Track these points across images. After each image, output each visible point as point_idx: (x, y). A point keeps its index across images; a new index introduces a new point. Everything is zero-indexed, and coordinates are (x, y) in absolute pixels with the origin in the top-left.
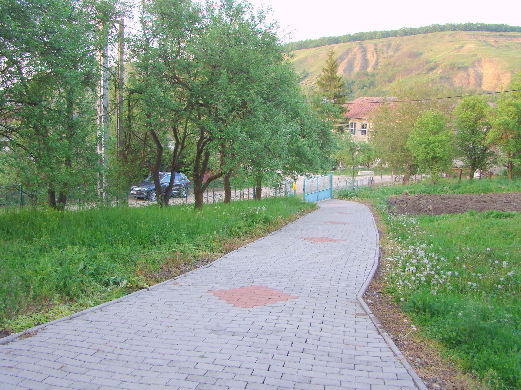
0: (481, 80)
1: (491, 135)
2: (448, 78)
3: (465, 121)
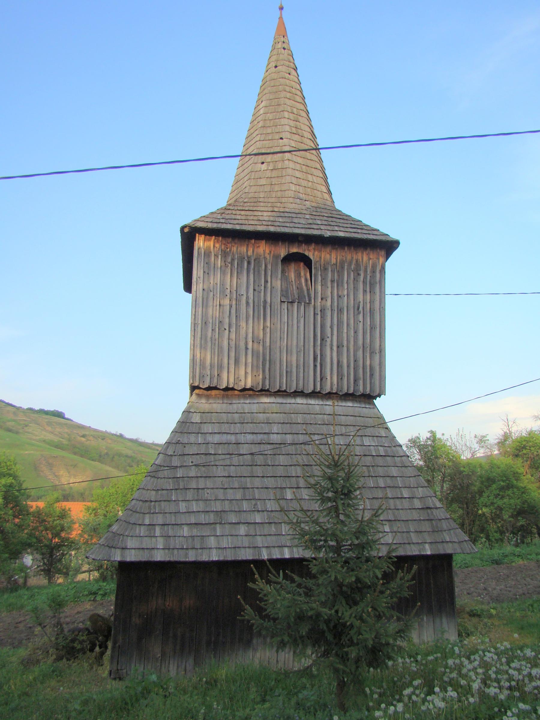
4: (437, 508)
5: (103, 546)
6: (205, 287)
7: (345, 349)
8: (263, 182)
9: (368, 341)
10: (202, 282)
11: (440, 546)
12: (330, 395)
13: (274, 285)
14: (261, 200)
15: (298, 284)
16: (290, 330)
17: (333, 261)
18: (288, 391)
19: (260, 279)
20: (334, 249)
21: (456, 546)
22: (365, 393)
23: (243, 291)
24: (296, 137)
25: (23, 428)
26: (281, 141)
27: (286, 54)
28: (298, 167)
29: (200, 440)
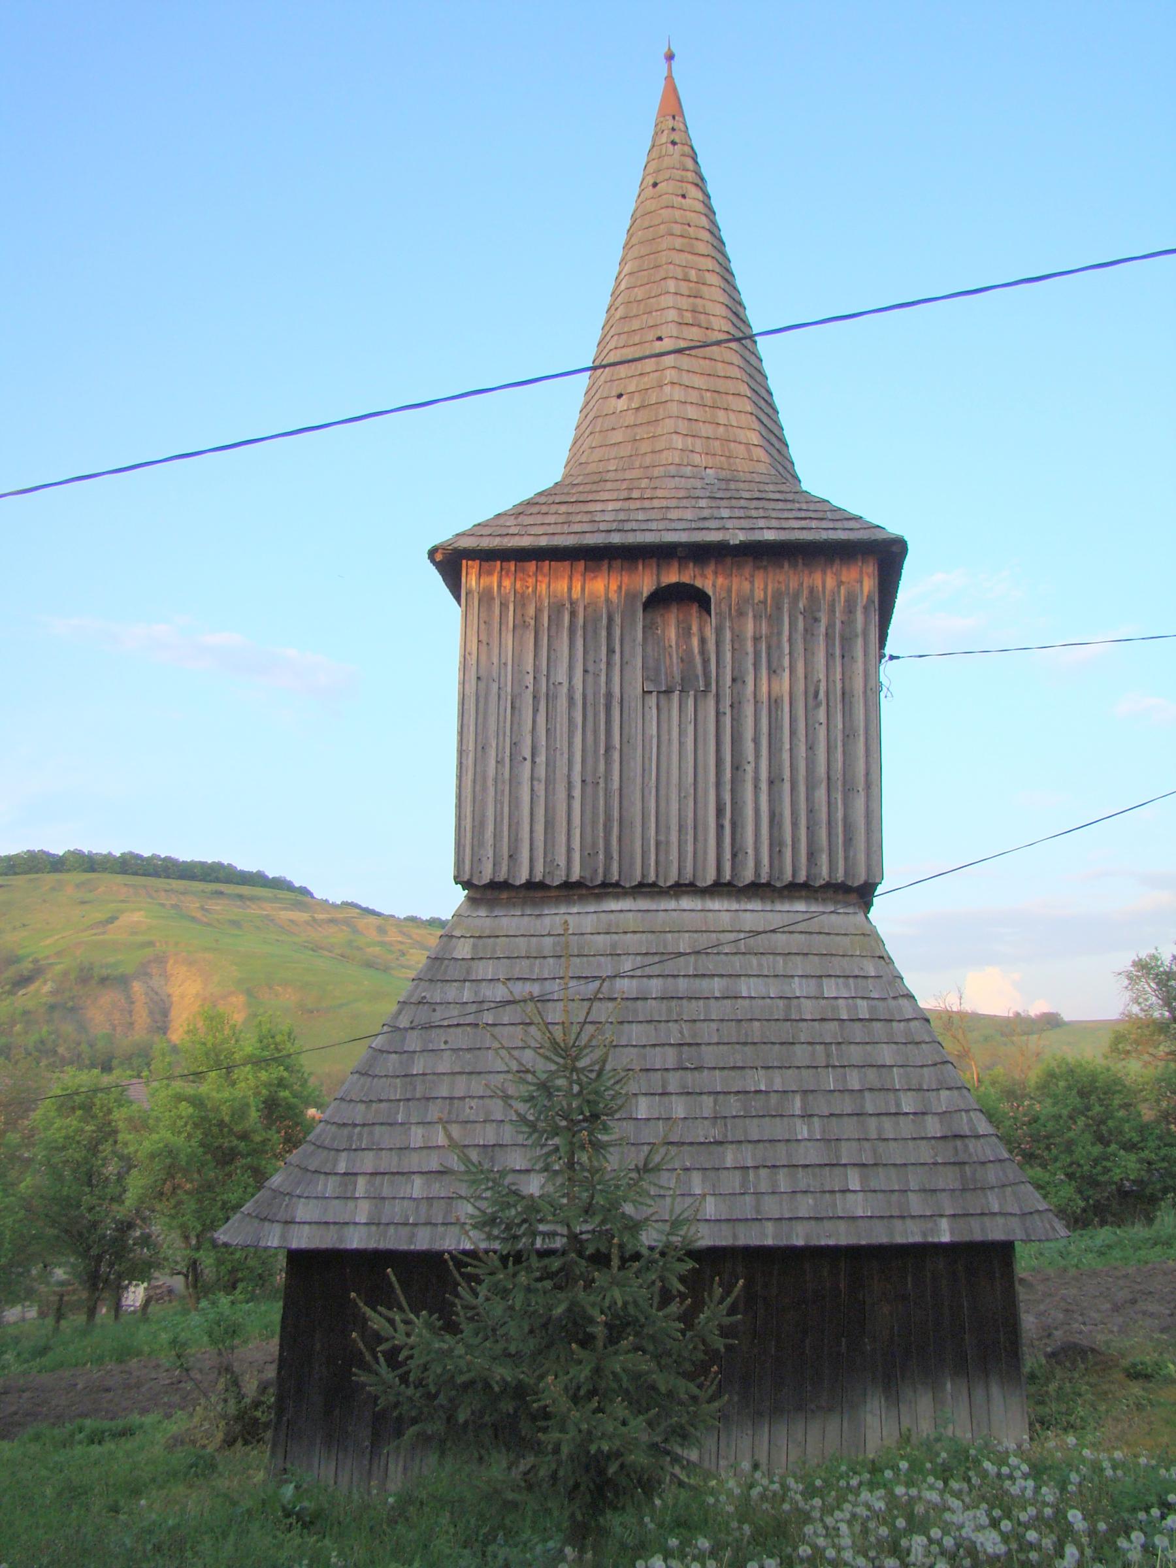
0: (165, 1013)
1: (136, 1185)
2: (72, 1009)
3: (64, 1148)
4: (978, 1137)
5: (248, 1219)
6: (483, 673)
7: (787, 786)
8: (617, 436)
9: (840, 765)
11: (975, 1224)
12: (756, 889)
15: (685, 650)
16: (664, 749)
17: (759, 595)
18: (661, 883)
19: (597, 649)
20: (758, 568)
21: (1015, 1223)
22: (834, 882)
23: (561, 676)
25: (397, 959)
26: (658, 343)
27: (676, 156)
28: (694, 396)
29: (467, 996)
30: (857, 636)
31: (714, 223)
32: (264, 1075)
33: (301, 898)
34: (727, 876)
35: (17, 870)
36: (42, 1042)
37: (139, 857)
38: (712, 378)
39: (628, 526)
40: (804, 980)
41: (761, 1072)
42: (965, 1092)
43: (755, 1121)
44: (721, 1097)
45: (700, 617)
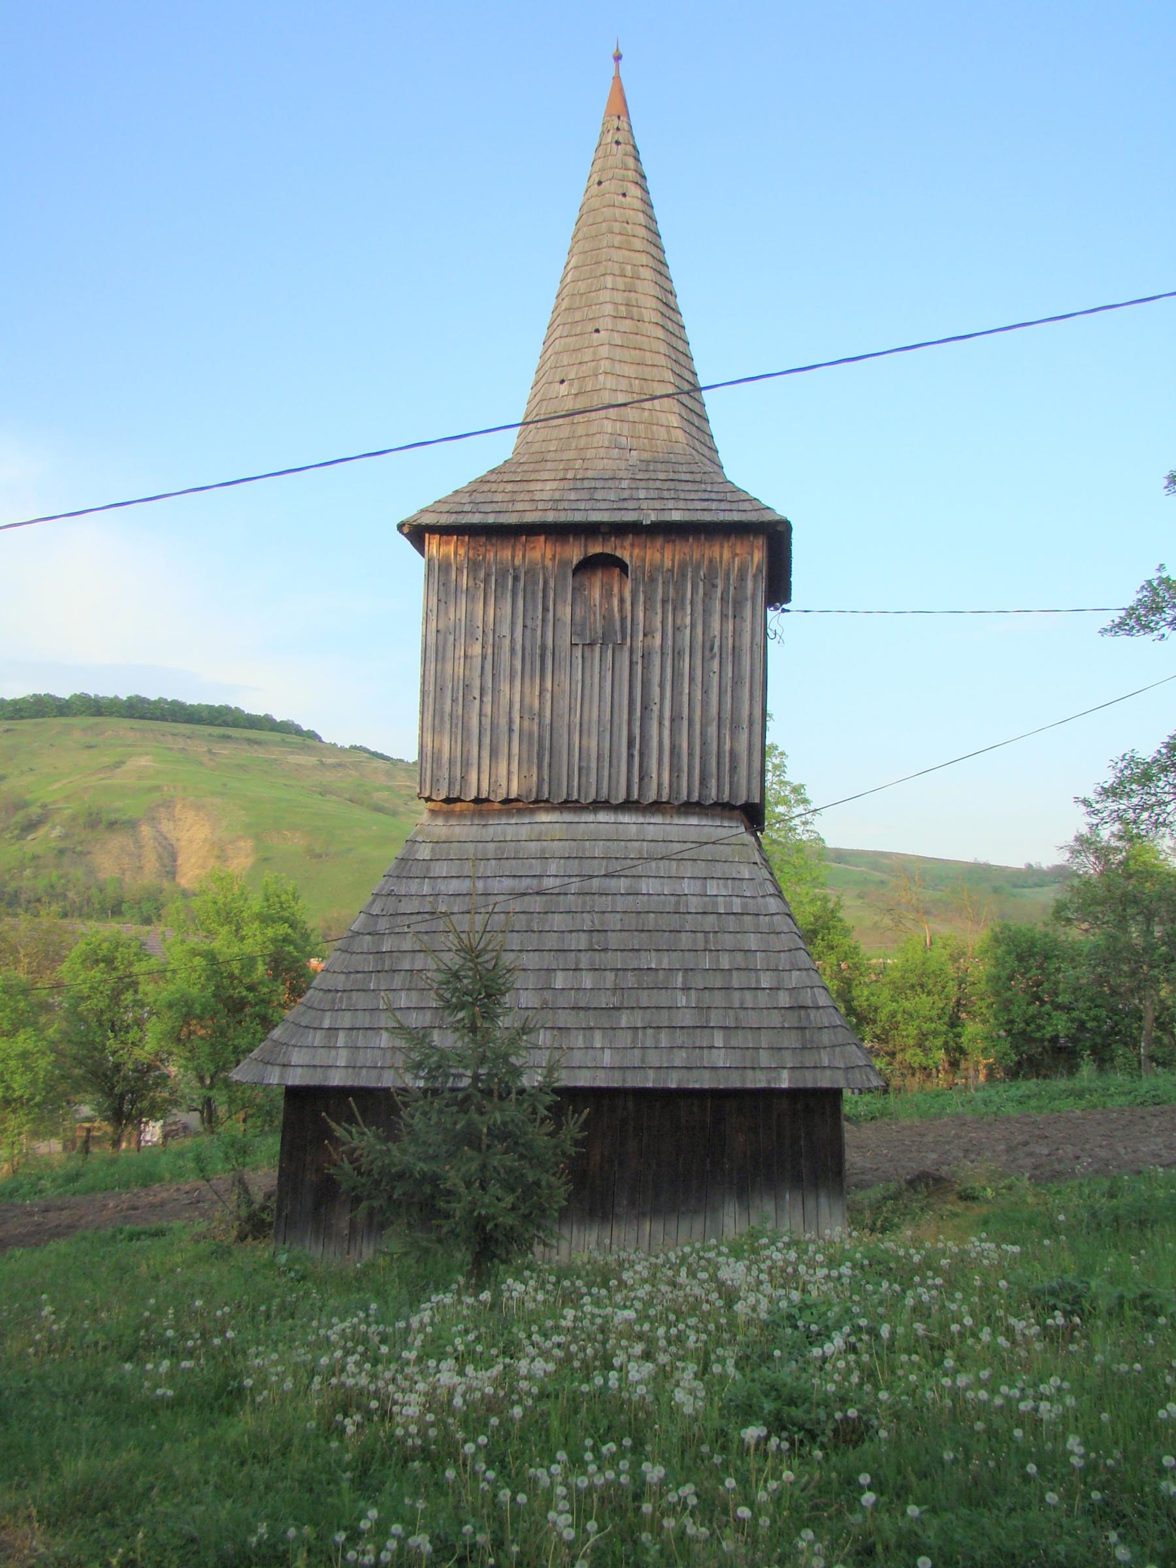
3: (89, 997)
4: (818, 1008)
6: (441, 627)
7: (685, 723)
9: (729, 706)
10: (435, 618)
11: (808, 1074)
12: (657, 807)
13: (559, 614)
14: (550, 456)
16: (587, 692)
17: (668, 564)
23: (505, 630)
24: (627, 325)
26: (596, 335)
27: (619, 155)
29: (426, 889)
30: (746, 599)
31: (652, 219)
32: (270, 932)
33: (309, 742)
34: (635, 796)
35: (23, 714)
36: (52, 886)
37: (144, 701)
38: (640, 367)
39: (561, 506)
40: (692, 881)
41: (653, 954)
42: (812, 973)
43: (646, 992)
44: (621, 973)
45: (620, 576)
